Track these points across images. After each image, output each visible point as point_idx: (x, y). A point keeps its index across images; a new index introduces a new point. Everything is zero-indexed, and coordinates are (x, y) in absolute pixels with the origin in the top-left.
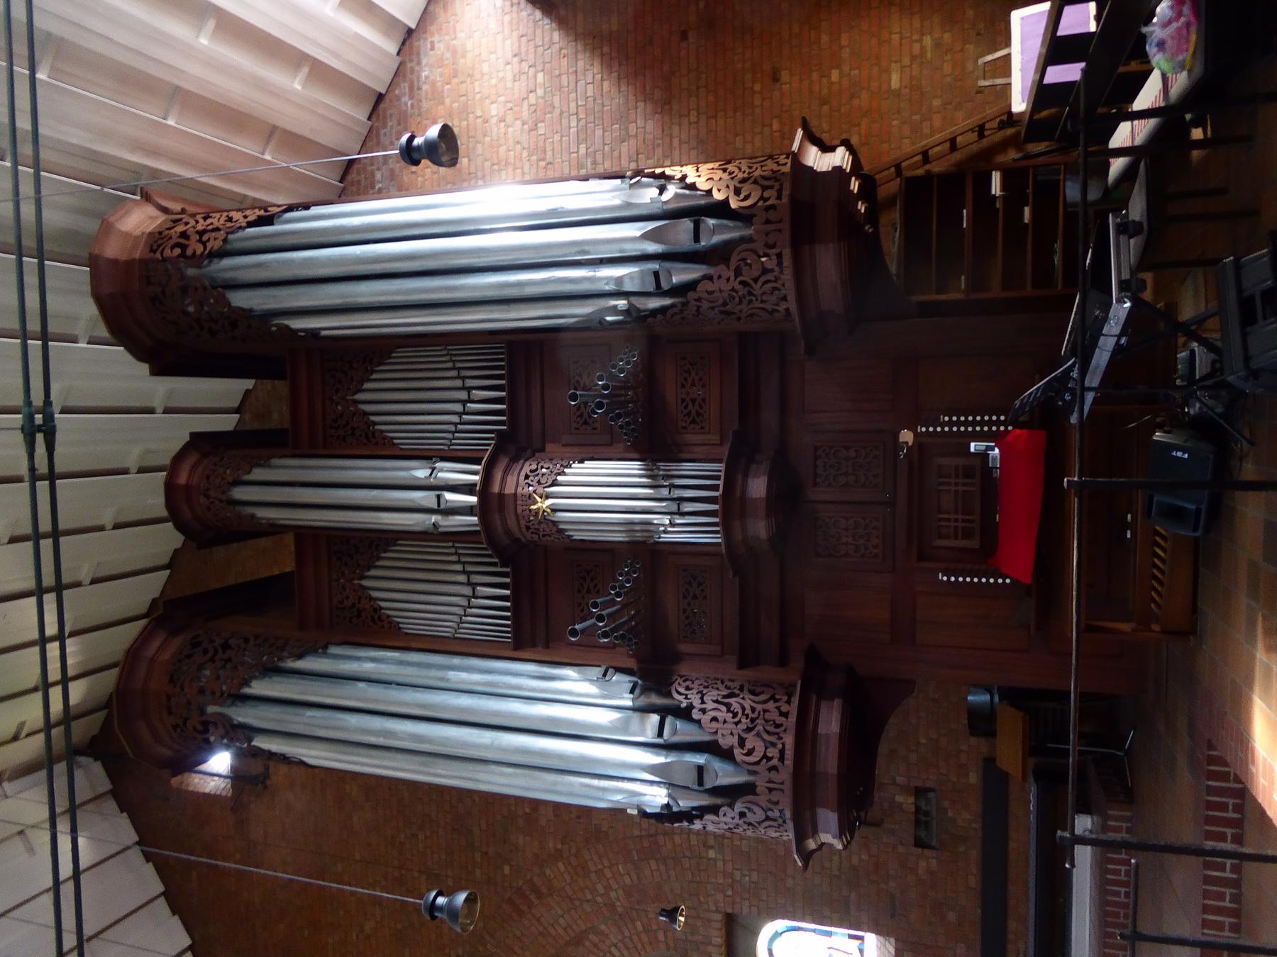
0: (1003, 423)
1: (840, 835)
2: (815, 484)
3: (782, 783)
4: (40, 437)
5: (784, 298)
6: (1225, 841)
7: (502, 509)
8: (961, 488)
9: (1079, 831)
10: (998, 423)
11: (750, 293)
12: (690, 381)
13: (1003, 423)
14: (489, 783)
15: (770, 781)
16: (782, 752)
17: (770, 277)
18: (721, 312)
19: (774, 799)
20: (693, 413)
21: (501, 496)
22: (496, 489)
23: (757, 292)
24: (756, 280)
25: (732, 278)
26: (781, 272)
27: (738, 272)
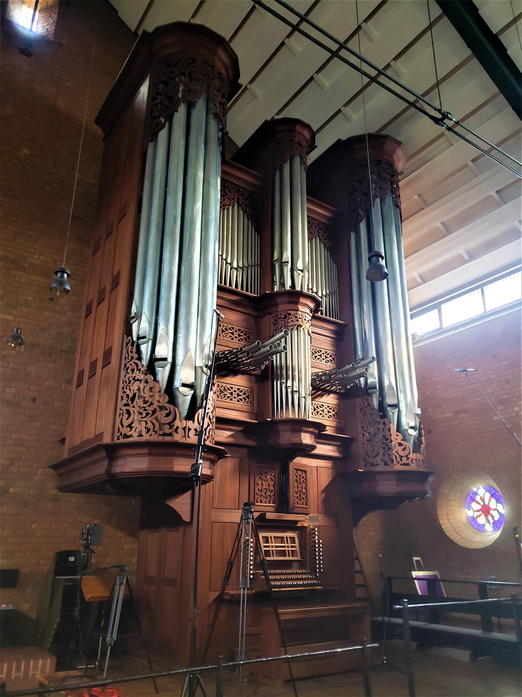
0: (320, 570)
1: (210, 468)
2: (258, 467)
3: (189, 437)
4: (439, 116)
5: (386, 464)
6: (15, 672)
7: (290, 303)
8: (286, 545)
9: (357, 582)
10: (320, 568)
11: (147, 414)
12: (240, 394)
13: (320, 570)
14: (213, 291)
15: (189, 429)
16: (408, 464)
17: (398, 459)
18: (135, 395)
19: (179, 431)
20: (225, 393)
21: (297, 303)
22: (302, 300)
23: (147, 419)
24: (157, 419)
25: (397, 441)
26: (401, 465)
27: (161, 408)
